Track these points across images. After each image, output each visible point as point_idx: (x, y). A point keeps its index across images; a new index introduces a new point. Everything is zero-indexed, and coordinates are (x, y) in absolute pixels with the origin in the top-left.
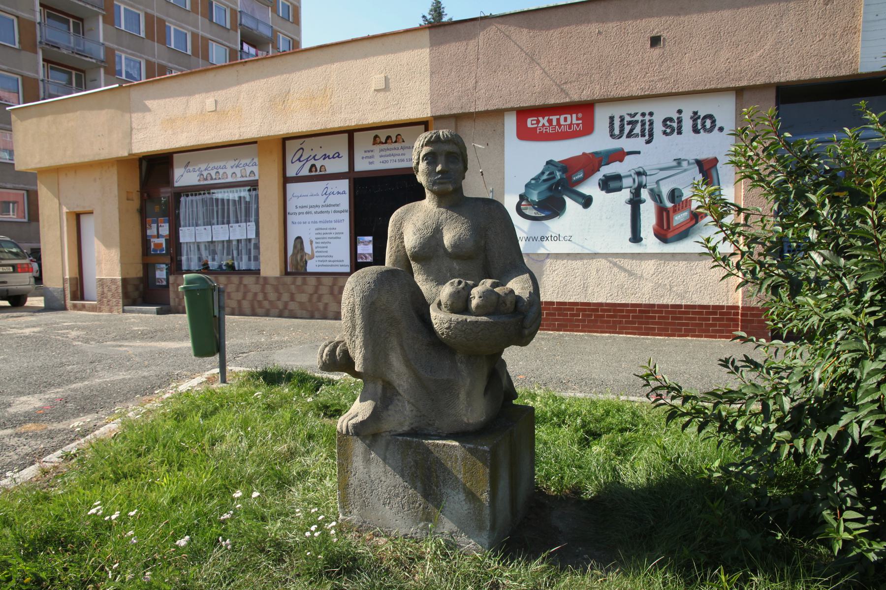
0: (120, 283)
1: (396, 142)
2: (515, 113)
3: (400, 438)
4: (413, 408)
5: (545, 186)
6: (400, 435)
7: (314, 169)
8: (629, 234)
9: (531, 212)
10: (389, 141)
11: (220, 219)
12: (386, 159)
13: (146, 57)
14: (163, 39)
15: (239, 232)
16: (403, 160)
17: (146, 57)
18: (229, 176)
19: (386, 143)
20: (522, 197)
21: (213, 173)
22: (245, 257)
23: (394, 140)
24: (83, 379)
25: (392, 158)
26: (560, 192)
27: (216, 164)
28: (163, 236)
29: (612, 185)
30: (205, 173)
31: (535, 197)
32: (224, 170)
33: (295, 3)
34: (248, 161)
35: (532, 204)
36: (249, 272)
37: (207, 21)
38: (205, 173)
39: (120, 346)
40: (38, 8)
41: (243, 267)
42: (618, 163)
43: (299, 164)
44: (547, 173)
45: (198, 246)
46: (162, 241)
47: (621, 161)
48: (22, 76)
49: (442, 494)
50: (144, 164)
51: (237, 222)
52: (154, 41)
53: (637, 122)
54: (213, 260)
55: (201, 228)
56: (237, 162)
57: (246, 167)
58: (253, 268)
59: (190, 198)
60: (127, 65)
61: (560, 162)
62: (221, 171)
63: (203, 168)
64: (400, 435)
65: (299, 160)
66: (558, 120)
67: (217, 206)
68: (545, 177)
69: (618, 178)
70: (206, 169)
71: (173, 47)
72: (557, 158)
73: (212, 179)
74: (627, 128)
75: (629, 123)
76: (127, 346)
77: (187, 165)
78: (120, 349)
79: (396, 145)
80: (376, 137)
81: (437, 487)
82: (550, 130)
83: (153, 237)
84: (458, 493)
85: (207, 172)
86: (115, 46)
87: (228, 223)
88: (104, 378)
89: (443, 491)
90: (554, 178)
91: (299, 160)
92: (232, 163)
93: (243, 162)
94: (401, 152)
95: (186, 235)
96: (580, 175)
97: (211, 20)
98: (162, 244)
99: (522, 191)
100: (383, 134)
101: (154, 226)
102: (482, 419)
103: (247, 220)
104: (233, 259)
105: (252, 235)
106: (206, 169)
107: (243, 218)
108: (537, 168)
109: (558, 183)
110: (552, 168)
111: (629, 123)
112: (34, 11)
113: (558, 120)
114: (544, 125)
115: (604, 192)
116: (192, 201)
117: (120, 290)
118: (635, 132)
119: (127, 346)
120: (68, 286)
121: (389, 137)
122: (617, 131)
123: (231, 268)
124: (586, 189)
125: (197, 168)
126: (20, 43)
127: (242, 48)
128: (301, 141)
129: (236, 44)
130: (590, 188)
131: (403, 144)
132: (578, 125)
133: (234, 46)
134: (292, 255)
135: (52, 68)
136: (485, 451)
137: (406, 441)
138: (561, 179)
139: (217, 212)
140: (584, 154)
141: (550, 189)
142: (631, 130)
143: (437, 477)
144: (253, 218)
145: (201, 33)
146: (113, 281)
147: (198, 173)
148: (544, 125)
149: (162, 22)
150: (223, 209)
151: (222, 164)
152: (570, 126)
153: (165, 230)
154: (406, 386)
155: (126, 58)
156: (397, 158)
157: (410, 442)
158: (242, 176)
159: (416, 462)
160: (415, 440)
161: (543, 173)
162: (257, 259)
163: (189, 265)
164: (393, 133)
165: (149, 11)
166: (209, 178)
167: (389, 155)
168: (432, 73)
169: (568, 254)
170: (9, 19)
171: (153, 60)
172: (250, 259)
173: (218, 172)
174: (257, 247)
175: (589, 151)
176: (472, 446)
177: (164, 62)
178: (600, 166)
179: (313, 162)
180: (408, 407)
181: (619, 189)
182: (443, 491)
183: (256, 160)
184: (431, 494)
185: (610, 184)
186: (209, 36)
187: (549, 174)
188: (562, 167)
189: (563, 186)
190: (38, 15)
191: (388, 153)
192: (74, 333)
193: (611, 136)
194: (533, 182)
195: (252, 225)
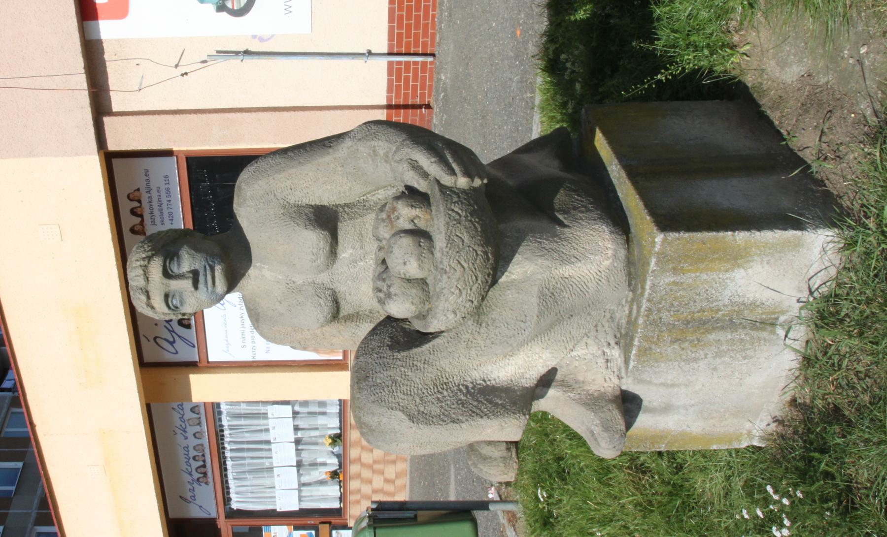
1: (139, 201)
2: (85, 23)
3: (632, 364)
4: (582, 344)
7: (186, 322)
10: (139, 211)
12: (166, 215)
13: (30, 526)
15: (280, 428)
17: (30, 526)
18: (199, 442)
19: (141, 216)
22: (321, 421)
23: (136, 204)
25: (164, 207)
27: (183, 459)
30: (196, 475)
32: (191, 448)
34: (176, 416)
38: (196, 475)
41: (336, 422)
43: (179, 342)
45: (304, 485)
49: (732, 303)
51: (267, 430)
52: (6, 514)
54: (324, 464)
55: (277, 481)
56: (179, 432)
57: (186, 417)
58: (336, 409)
59: (226, 445)
62: (193, 453)
63: (188, 478)
64: (627, 362)
65: (172, 343)
67: (244, 458)
70: (191, 474)
71: (13, 488)
73: (204, 466)
77: (185, 500)
80: (133, 231)
81: (719, 310)
84: (733, 280)
85: (194, 473)
89: (726, 301)
91: (172, 343)
92: (180, 438)
93: (178, 423)
94: (154, 194)
100: (129, 221)
103: (265, 416)
104: (323, 436)
106: (191, 474)
107: (262, 422)
116: (237, 493)
121: (133, 212)
123: (336, 439)
125: (190, 487)
127: (9, 390)
128: (143, 340)
129: (4, 398)
131: (143, 191)
133: (7, 401)
136: (665, 240)
137: (637, 355)
139: (252, 458)
143: (702, 310)
144: (262, 409)
147: (195, 485)
150: (249, 450)
151: (181, 452)
154: (547, 355)
156: (164, 199)
157: (639, 350)
158: (199, 424)
159: (673, 342)
160: (636, 343)
162: (322, 404)
163: (333, 499)
164: (125, 206)
166: (203, 470)
167: (161, 210)
168: (31, 154)
172: (324, 414)
173: (194, 458)
174: (305, 403)
177: (36, 502)
179: (175, 325)
180: (580, 351)
182: (726, 301)
184: (731, 320)
195: (272, 410)
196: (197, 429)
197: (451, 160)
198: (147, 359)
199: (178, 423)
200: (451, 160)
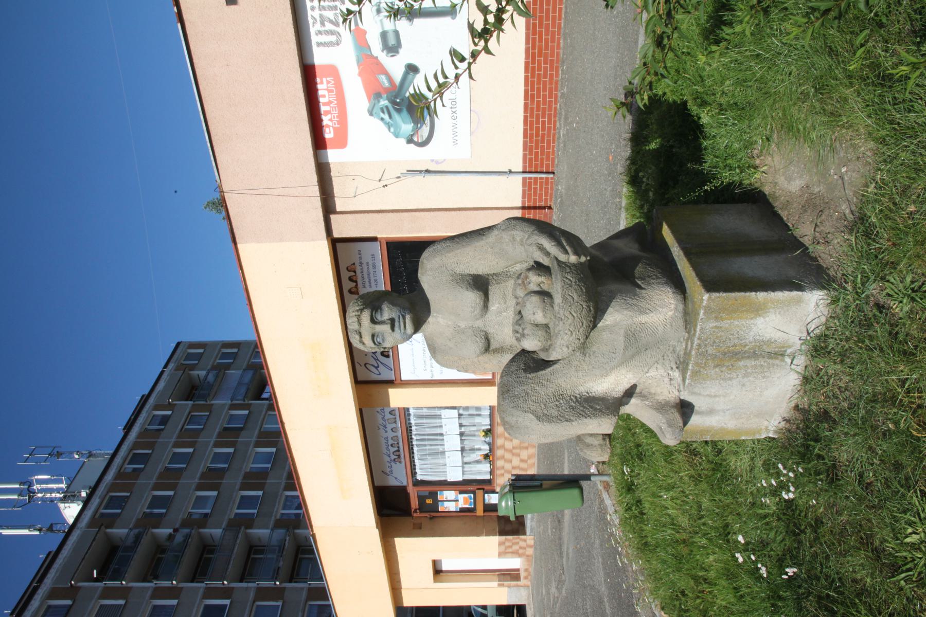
0: (503, 538)
1: (355, 272)
3: (687, 382)
4: (654, 368)
5: (395, 115)
6: (684, 380)
8: (447, 20)
9: (425, 131)
10: (354, 278)
11: (439, 443)
14: (264, 474)
15: (450, 425)
16: (374, 264)
18: (395, 434)
19: (356, 282)
20: (410, 141)
21: (392, 449)
22: (477, 420)
23: (353, 274)
24: (601, 602)
25: (372, 275)
26: (402, 100)
27: (384, 446)
28: (457, 497)
29: (392, 41)
30: (393, 457)
31: (407, 127)
33: (219, 347)
34: (380, 417)
35: (416, 130)
36: (491, 416)
37: (243, 433)
38: (393, 457)
39: (568, 554)
40: (244, 585)
42: (367, 36)
43: (381, 368)
44: (382, 115)
45: (466, 463)
46: (461, 497)
47: (365, 32)
48: (306, 602)
49: (755, 341)
50: (386, 511)
51: (441, 426)
53: (321, 16)
55: (448, 461)
56: (381, 427)
57: (386, 418)
58: (488, 412)
60: (290, 509)
61: (369, 100)
62: (391, 442)
63: (388, 459)
64: (684, 380)
65: (377, 368)
66: (325, 104)
67: (425, 445)
68: (386, 117)
69: (384, 35)
71: (269, 466)
72: (365, 104)
73: (398, 451)
74: (329, 27)
75: (323, 24)
76: (568, 549)
77: (385, 473)
78: (571, 555)
79: (360, 282)
80: (350, 292)
82: (335, 113)
83: (457, 505)
84: (755, 325)
86: (273, 518)
87: (443, 453)
88: (599, 578)
89: (751, 339)
90: (387, 107)
91: (377, 368)
92: (382, 431)
93: (381, 421)
95: (455, 475)
96: (383, 79)
97: (241, 429)
98: (464, 498)
99: (403, 141)
100: (347, 285)
101: (446, 504)
102: (671, 294)
103: (439, 417)
105: (455, 413)
107: (437, 421)
108: (376, 126)
109: (394, 103)
110: (377, 110)
111: (323, 24)
112: (247, 588)
113: (325, 104)
114: (331, 120)
115: (401, 51)
117: (511, 537)
118: (332, 18)
119: (568, 549)
120: (506, 583)
121: (351, 279)
122: (333, 38)
123: (488, 432)
124: (397, 73)
126: (276, 600)
127: (267, 399)
128: (357, 366)
129: (264, 404)
130: (395, 67)
131: (357, 264)
132: (328, 82)
134: (474, 373)
135: (298, 575)
136: (710, 298)
138: (388, 99)
140: (360, 74)
141: (399, 111)
142: (331, 22)
143: (735, 345)
144: (437, 412)
145: (254, 439)
146: (500, 544)
147: (393, 464)
148: (331, 120)
149: (247, 475)
151: (383, 441)
152: (330, 91)
153: (449, 494)
154: (630, 375)
155: (284, 509)
156: (371, 270)
158: (395, 422)
159: (715, 367)
160: (690, 367)
161: (382, 119)
162: (478, 409)
163: (485, 473)
164: (345, 275)
165: (237, 487)
167: (369, 278)
168: (281, 240)
169: (539, 488)
170: (256, 612)
171: (283, 484)
172: (479, 415)
174: (467, 408)
175: (355, 69)
176: (702, 312)
178: (372, 56)
180: (652, 373)
181: (397, 33)
182: (751, 339)
183: (379, 409)
184: (754, 352)
185: (392, 46)
186: (257, 432)
187: (383, 112)
188: (375, 99)
189: (396, 97)
190: (251, 585)
191: (366, 279)
192: (553, 590)
193: (338, 44)
194: (392, 130)
195: (444, 413)
196: (394, 425)
197: (565, 244)
198: (360, 378)
199: (381, 421)
200: (565, 244)
